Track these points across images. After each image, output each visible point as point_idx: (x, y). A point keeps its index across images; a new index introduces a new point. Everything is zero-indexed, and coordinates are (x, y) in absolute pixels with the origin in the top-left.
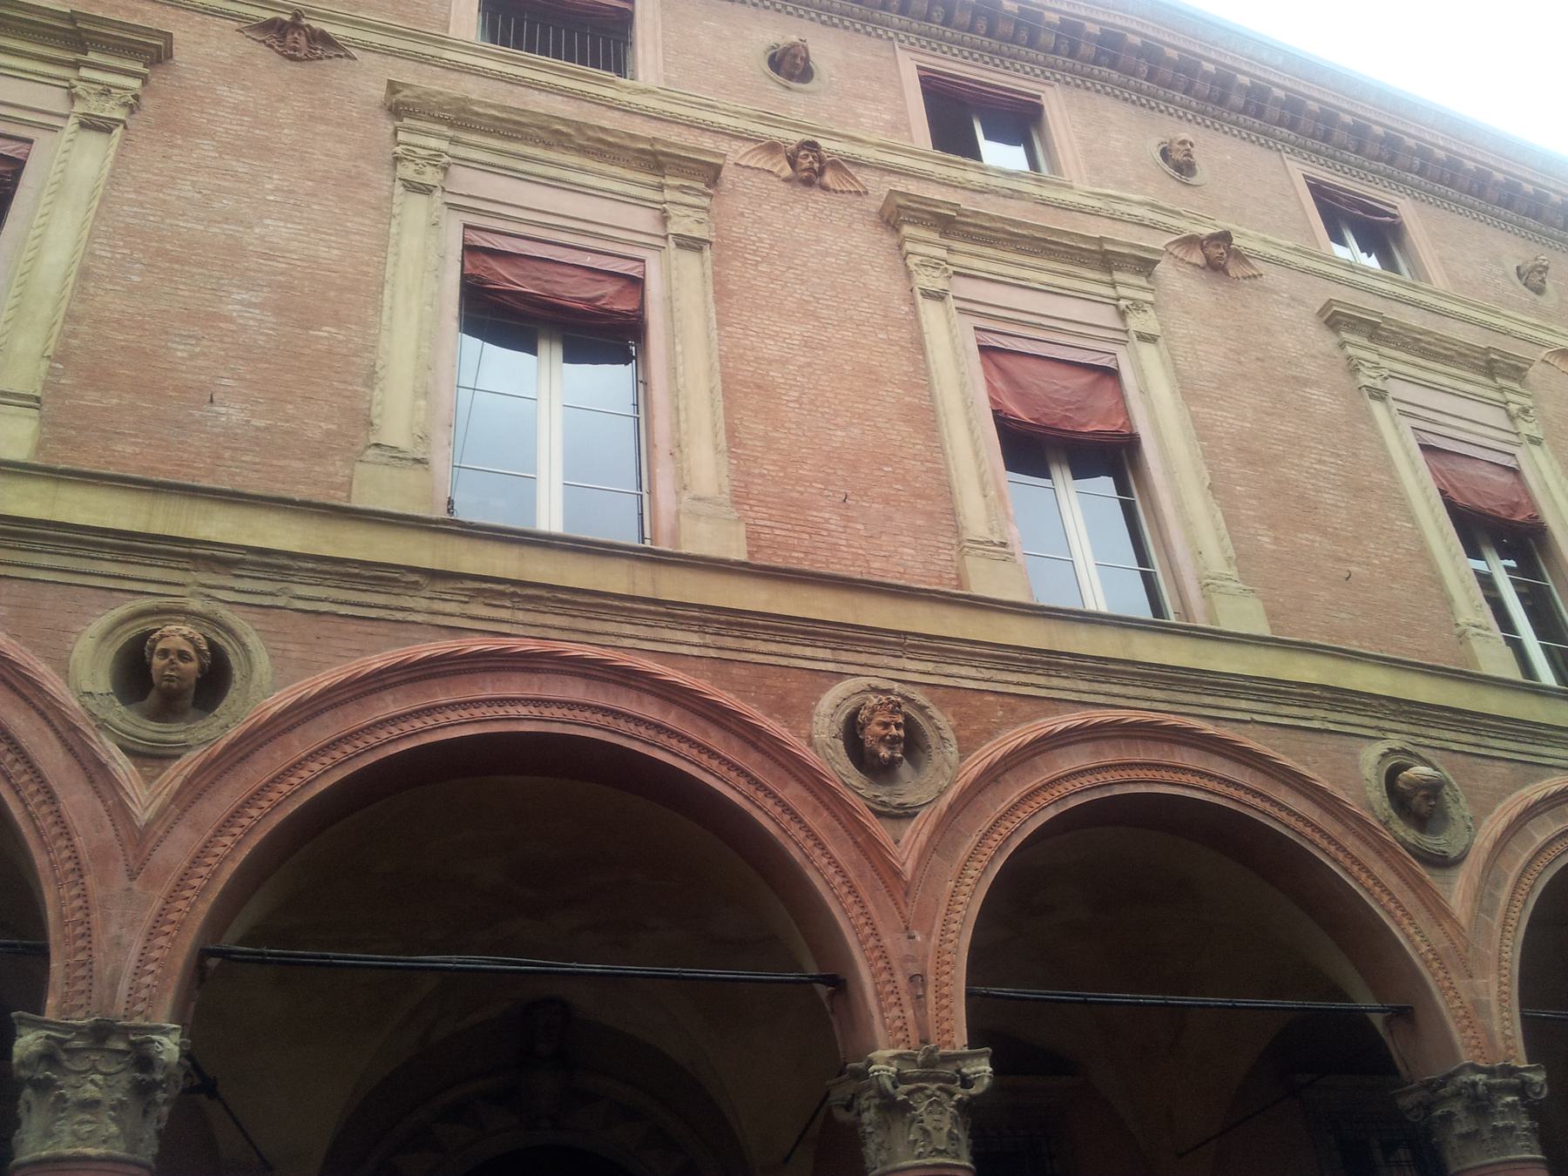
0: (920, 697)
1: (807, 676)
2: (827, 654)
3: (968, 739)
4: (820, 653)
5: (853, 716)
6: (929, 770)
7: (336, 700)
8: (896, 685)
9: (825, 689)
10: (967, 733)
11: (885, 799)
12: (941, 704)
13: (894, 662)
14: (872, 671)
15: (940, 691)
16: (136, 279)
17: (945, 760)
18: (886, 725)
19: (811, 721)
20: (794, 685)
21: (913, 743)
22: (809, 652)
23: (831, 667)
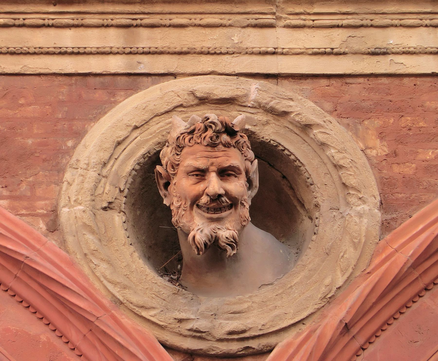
0: (303, 105)
1: (63, 90)
2: (113, 38)
3: (408, 182)
4: (92, 39)
5: (154, 159)
6: (310, 256)
7: (395, 246)
8: (254, 90)
9: (99, 111)
10: (409, 170)
11: (202, 324)
12: (351, 114)
13: (255, 39)
14: (206, 63)
15: (356, 89)
16: (409, 118)
17: (345, 229)
18: (201, 174)
19: (59, 183)
20: (32, 111)
21: (279, 198)
22: (68, 39)
23: (115, 64)
